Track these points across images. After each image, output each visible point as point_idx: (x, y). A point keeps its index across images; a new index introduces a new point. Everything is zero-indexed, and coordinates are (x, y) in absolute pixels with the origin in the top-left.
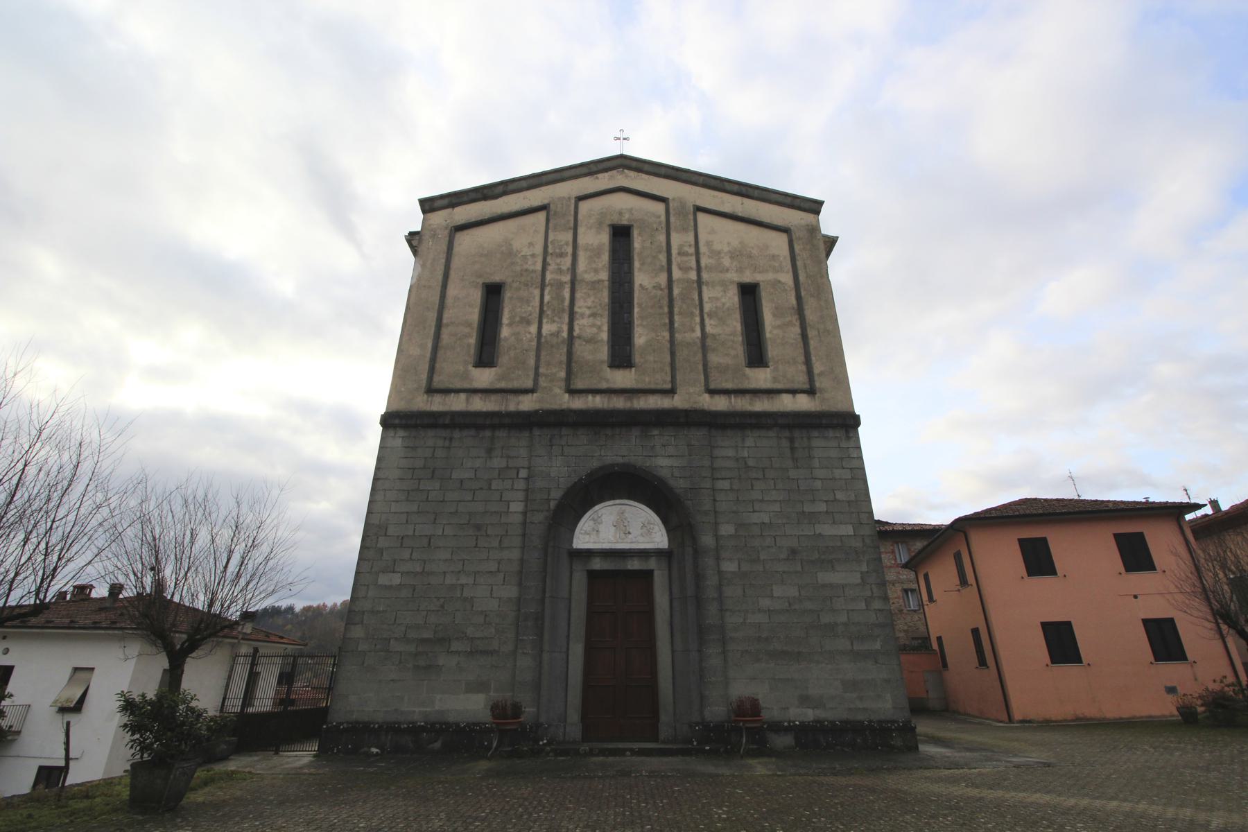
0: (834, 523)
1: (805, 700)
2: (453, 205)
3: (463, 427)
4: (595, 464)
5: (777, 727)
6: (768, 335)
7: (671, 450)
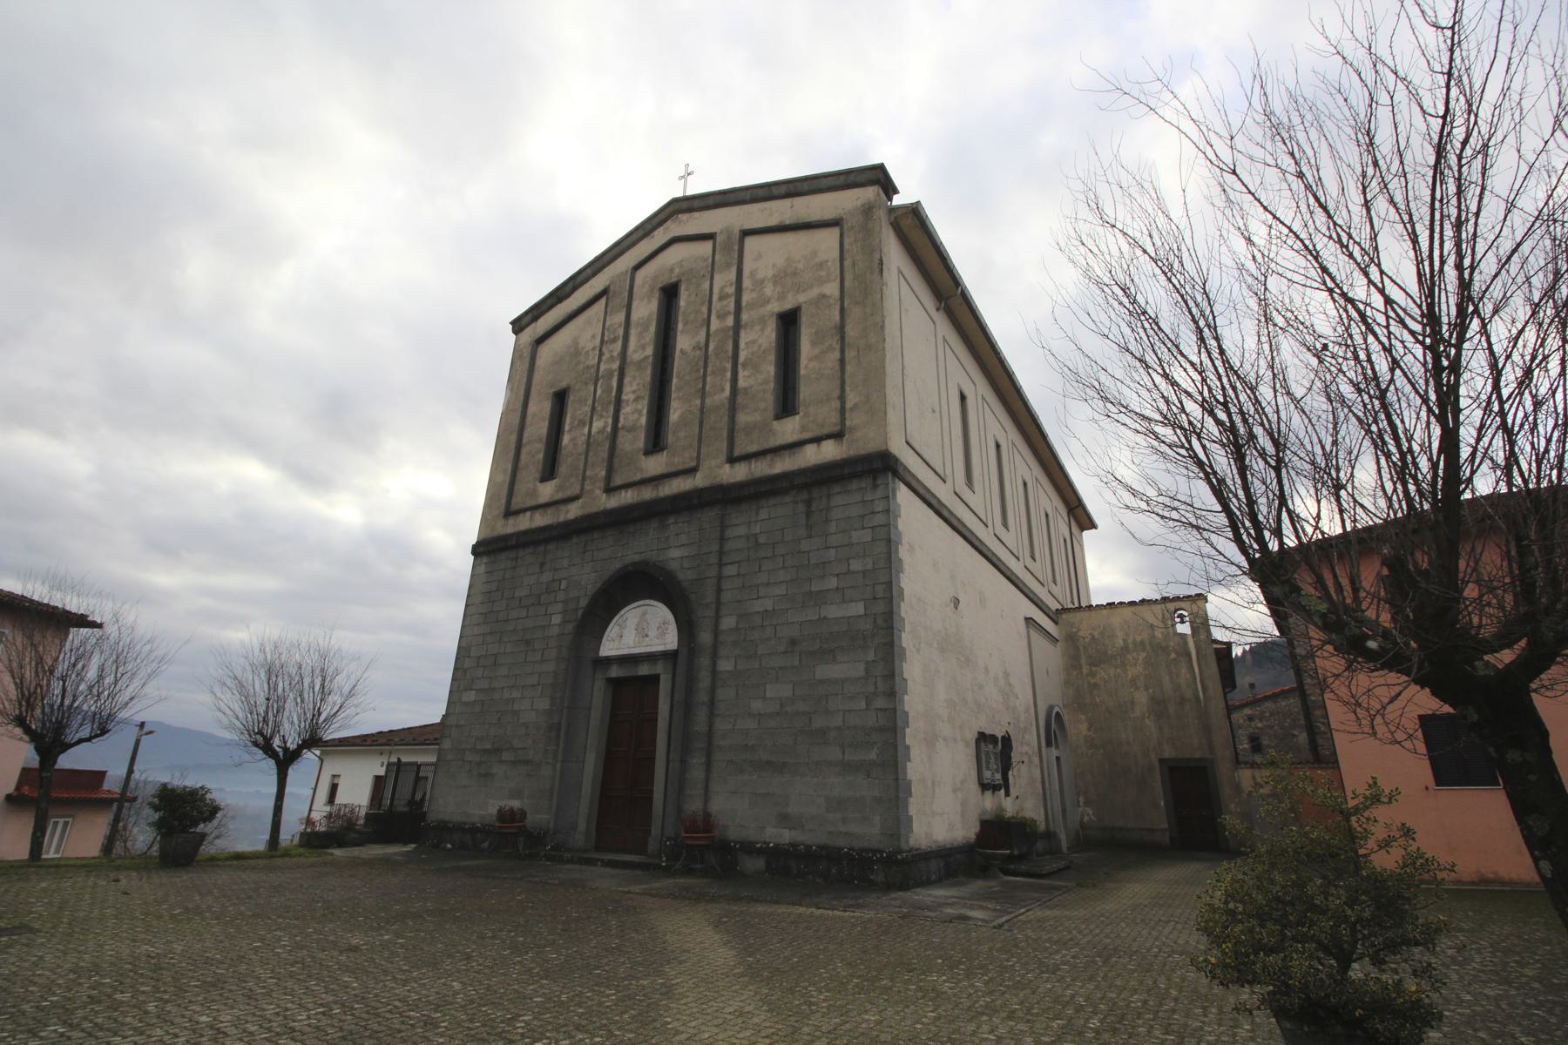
0: (844, 602)
1: (784, 819)
2: (535, 319)
3: (525, 545)
4: (617, 565)
5: (748, 848)
6: (802, 372)
7: (683, 539)
